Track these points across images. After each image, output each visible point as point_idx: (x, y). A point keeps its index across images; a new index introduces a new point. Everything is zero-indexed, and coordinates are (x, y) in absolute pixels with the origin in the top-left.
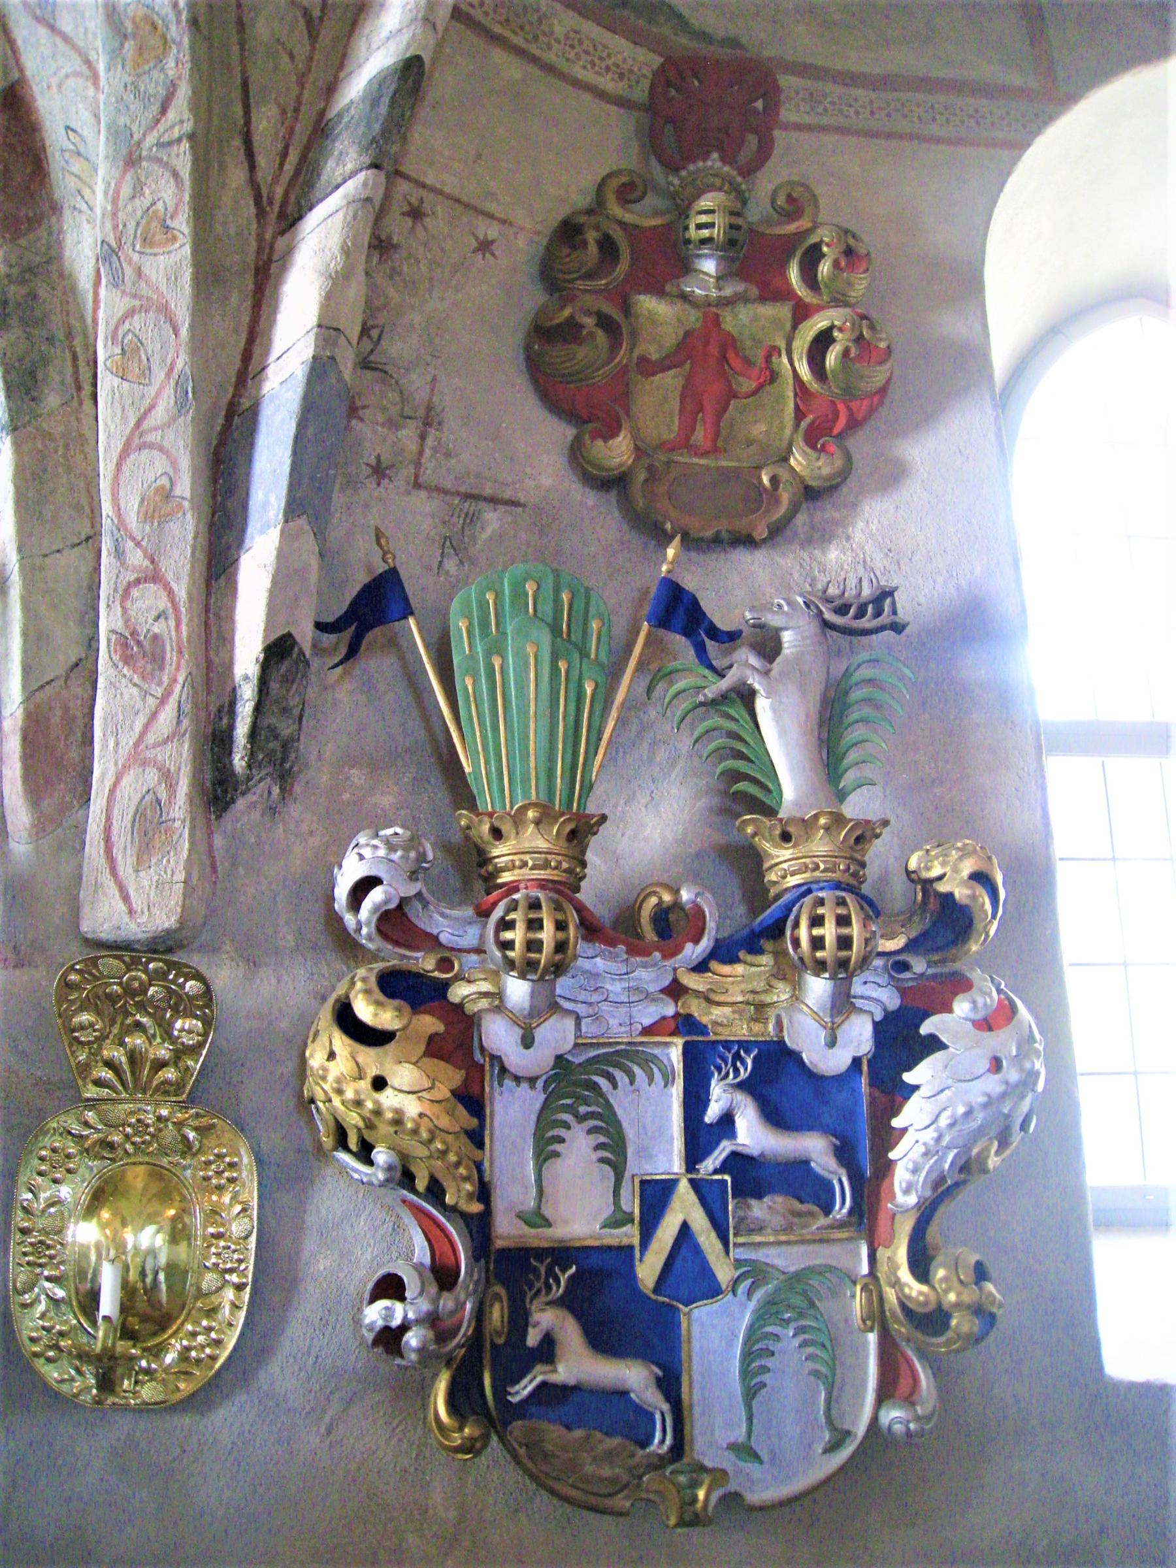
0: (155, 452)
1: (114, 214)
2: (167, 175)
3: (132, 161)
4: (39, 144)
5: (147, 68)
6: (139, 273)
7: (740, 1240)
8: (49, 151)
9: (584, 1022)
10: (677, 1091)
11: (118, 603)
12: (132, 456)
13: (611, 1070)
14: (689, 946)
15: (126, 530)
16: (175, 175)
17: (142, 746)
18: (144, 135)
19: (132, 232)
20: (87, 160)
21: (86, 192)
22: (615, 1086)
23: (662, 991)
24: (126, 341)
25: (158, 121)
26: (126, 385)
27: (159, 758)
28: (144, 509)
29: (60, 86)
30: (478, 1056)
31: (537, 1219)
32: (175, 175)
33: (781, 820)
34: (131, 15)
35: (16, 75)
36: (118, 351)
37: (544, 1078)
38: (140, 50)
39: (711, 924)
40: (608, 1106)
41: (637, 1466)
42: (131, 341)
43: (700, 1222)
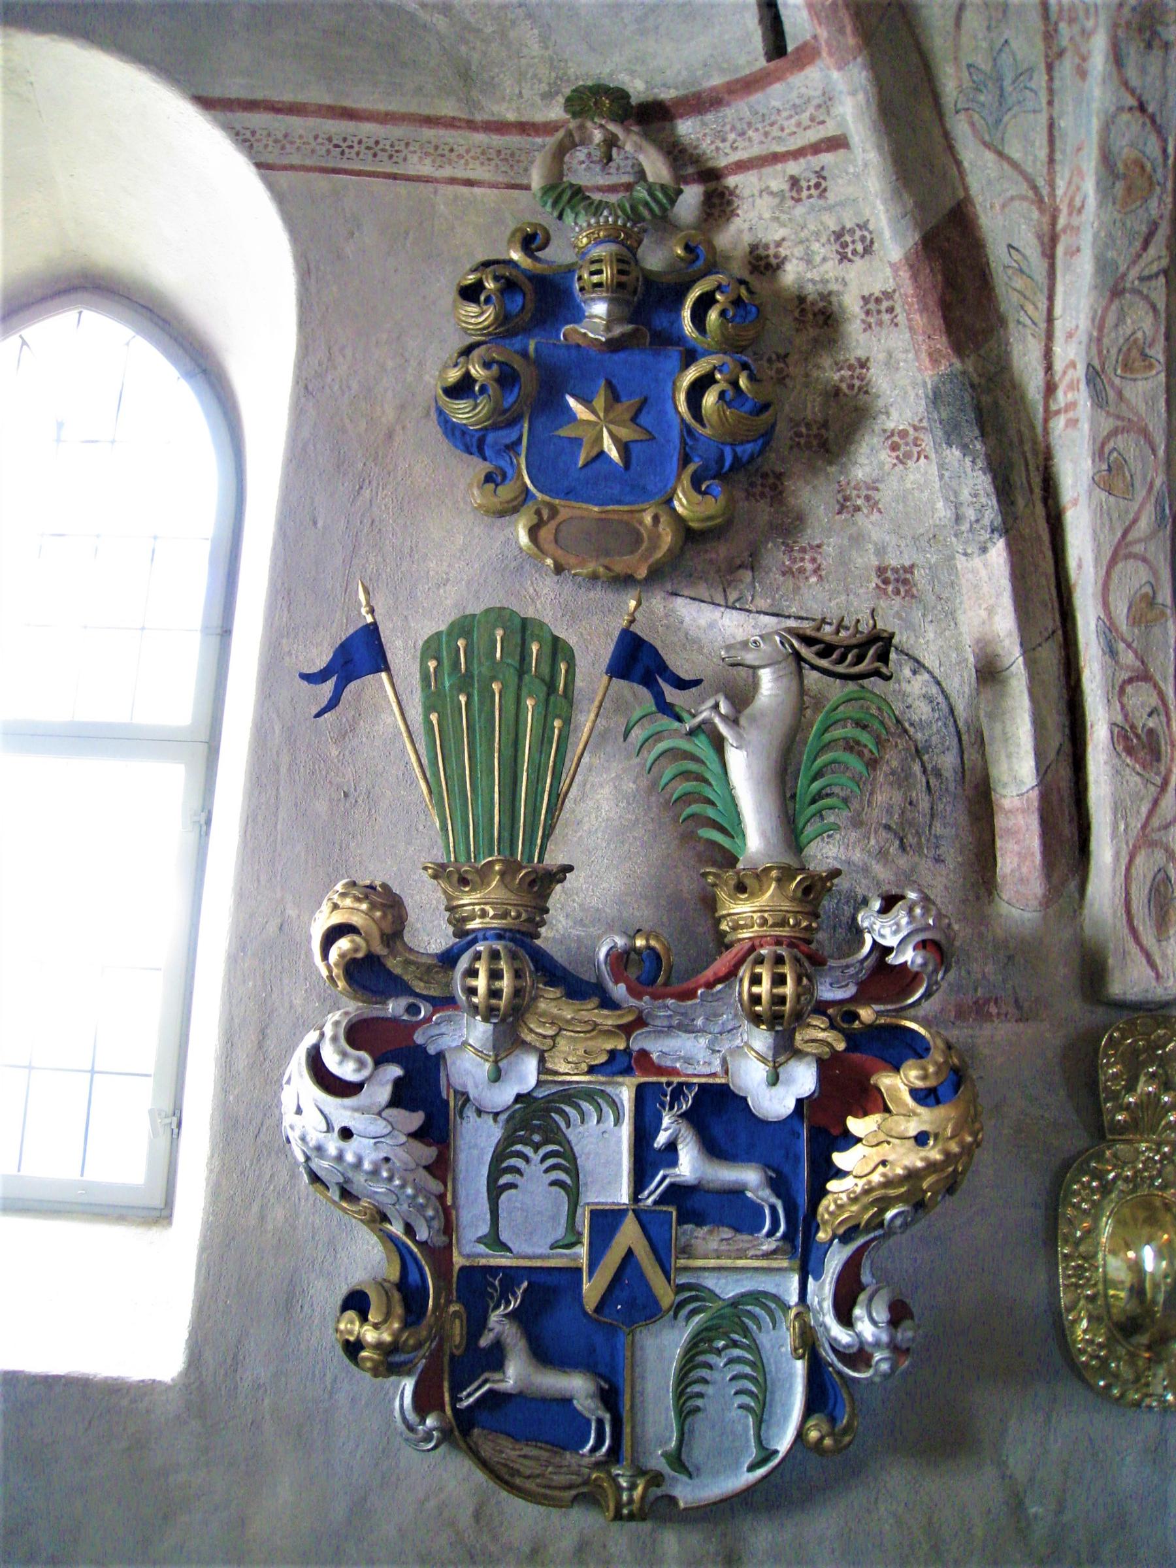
0: (1140, 563)
1: (1099, 340)
2: (1147, 307)
3: (1116, 292)
4: (984, 260)
5: (1134, 207)
6: (1120, 394)
8: (993, 265)
10: (626, 1131)
11: (1116, 698)
12: (1120, 565)
15: (1117, 631)
16: (1154, 308)
17: (1148, 830)
18: (1128, 269)
19: (1114, 358)
20: (1029, 277)
21: (1030, 308)
24: (1111, 459)
25: (1139, 256)
26: (1112, 499)
27: (1164, 839)
28: (1131, 616)
29: (1003, 206)
31: (494, 1240)
32: (1154, 308)
33: (738, 873)
34: (1124, 157)
35: (961, 194)
36: (1105, 467)
38: (1129, 190)
42: (1116, 459)
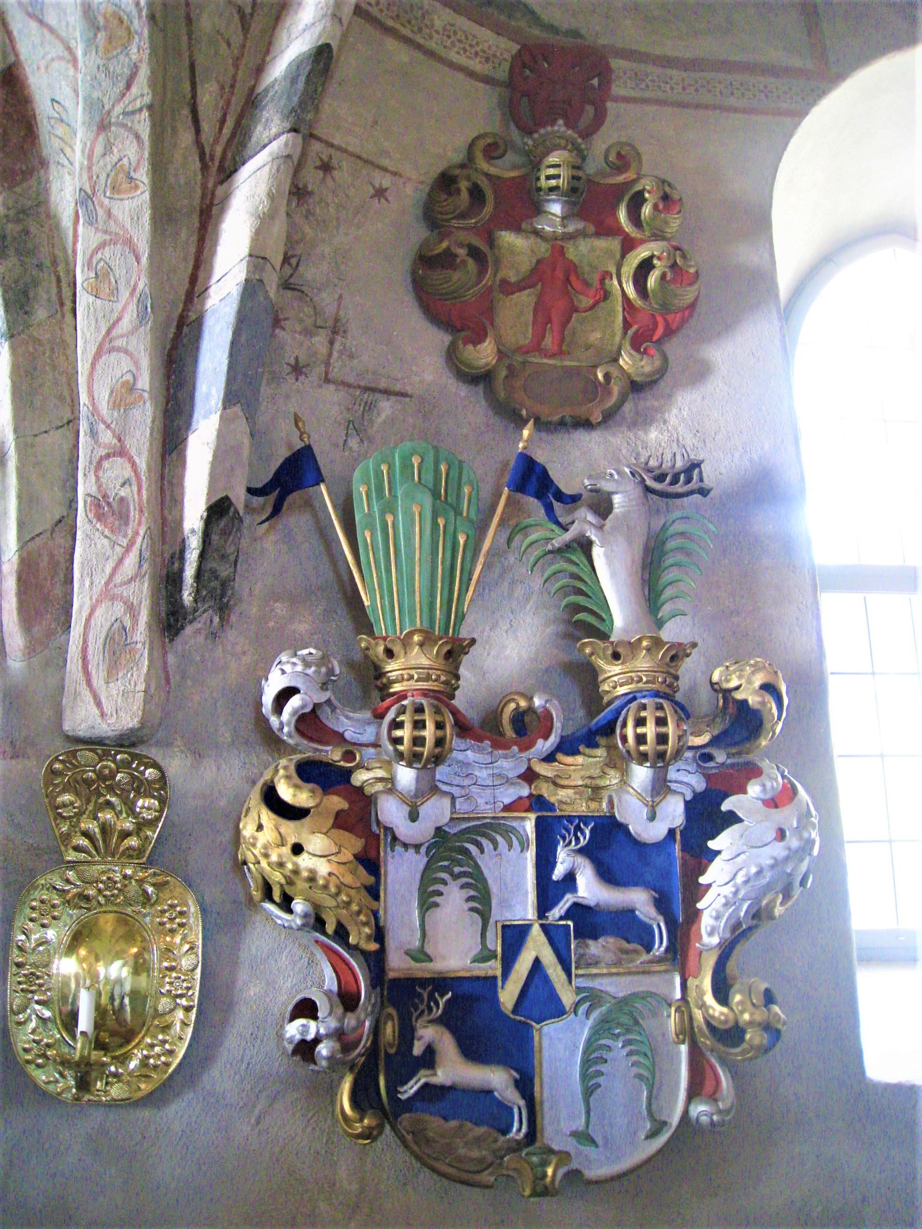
0: (122, 354)
1: (90, 168)
2: (131, 137)
3: (103, 126)
4: (31, 113)
5: (115, 53)
6: (109, 214)
7: (580, 972)
8: (39, 118)
9: (458, 801)
11: (92, 472)
12: (104, 358)
13: (479, 838)
14: (540, 742)
15: (99, 415)
16: (138, 137)
17: (112, 585)
18: (113, 106)
19: (103, 182)
20: (69, 125)
21: (68, 151)
22: (482, 851)
23: (519, 777)
24: (99, 267)
25: (124, 95)
26: (99, 301)
27: (125, 594)
28: (113, 399)
29: (47, 67)
30: (374, 828)
31: (421, 955)
32: (138, 137)
34: (103, 11)
35: (12, 59)
36: (93, 275)
37: (427, 845)
38: (110, 39)
39: (557, 725)
40: (477, 867)
41: (500, 1149)
42: (103, 268)
43: (548, 958)
